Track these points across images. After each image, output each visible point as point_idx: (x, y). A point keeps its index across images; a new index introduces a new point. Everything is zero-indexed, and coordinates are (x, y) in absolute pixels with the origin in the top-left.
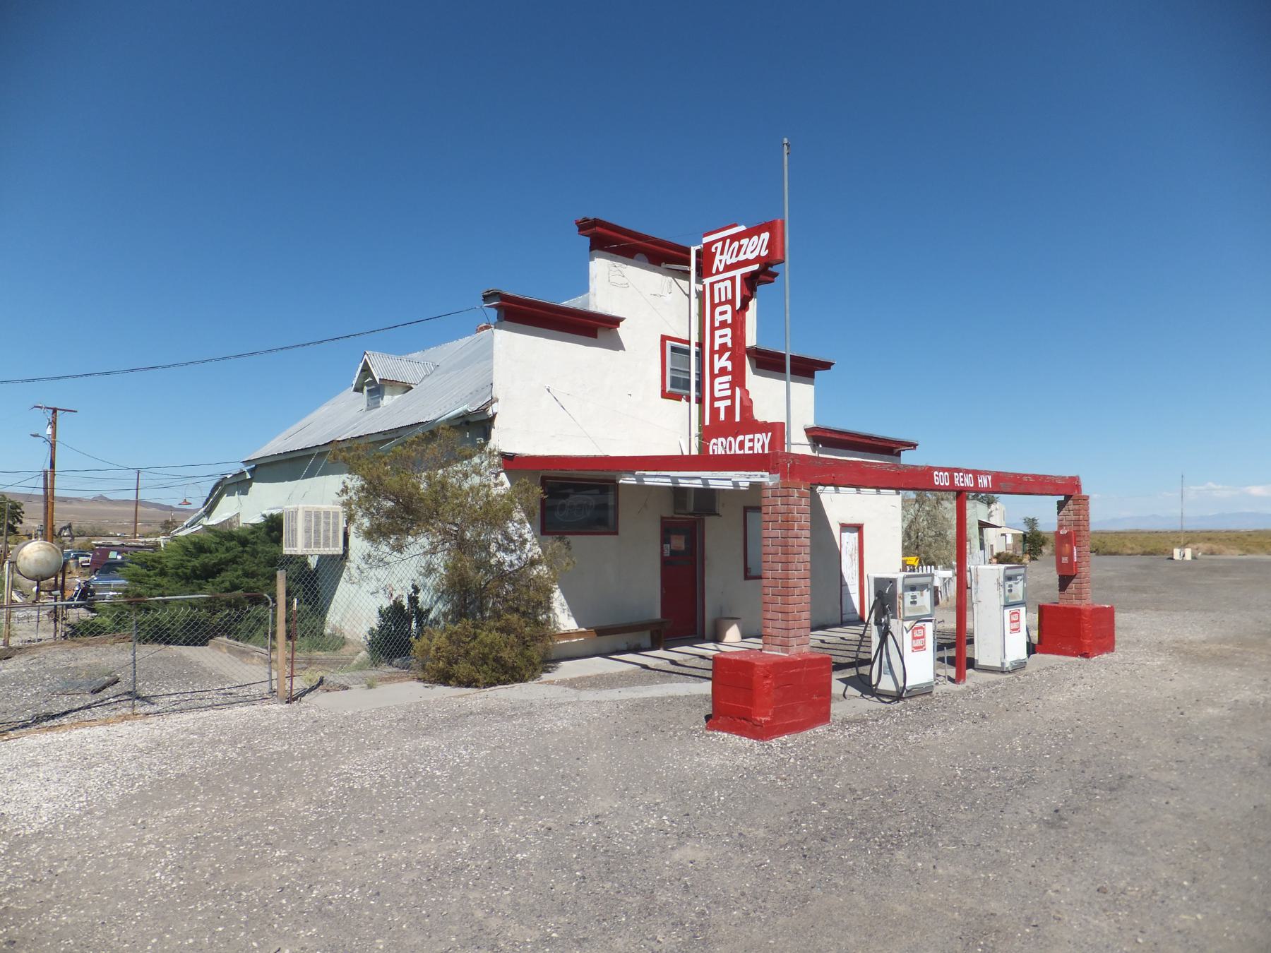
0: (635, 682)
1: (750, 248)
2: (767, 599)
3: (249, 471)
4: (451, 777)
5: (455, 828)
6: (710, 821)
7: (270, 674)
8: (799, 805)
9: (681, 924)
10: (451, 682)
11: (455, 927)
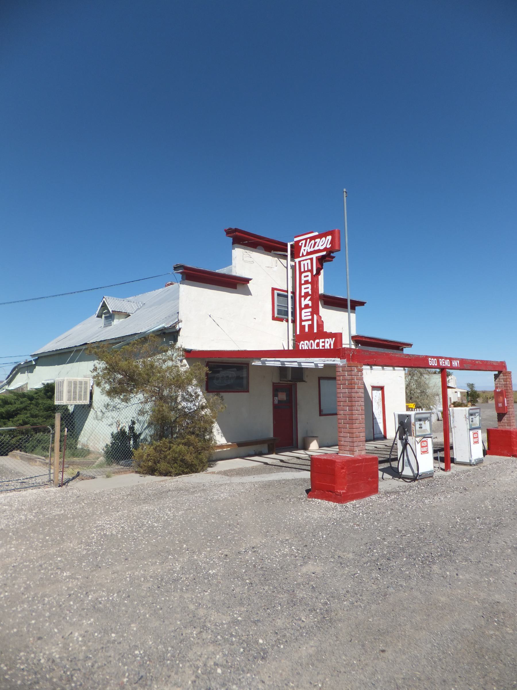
0: (246, 470)
1: (321, 244)
2: (341, 426)
3: (34, 360)
4: (164, 527)
5: (170, 556)
6: (320, 549)
7: (50, 471)
8: (370, 539)
9: (314, 610)
10: (155, 473)
11: (178, 615)
